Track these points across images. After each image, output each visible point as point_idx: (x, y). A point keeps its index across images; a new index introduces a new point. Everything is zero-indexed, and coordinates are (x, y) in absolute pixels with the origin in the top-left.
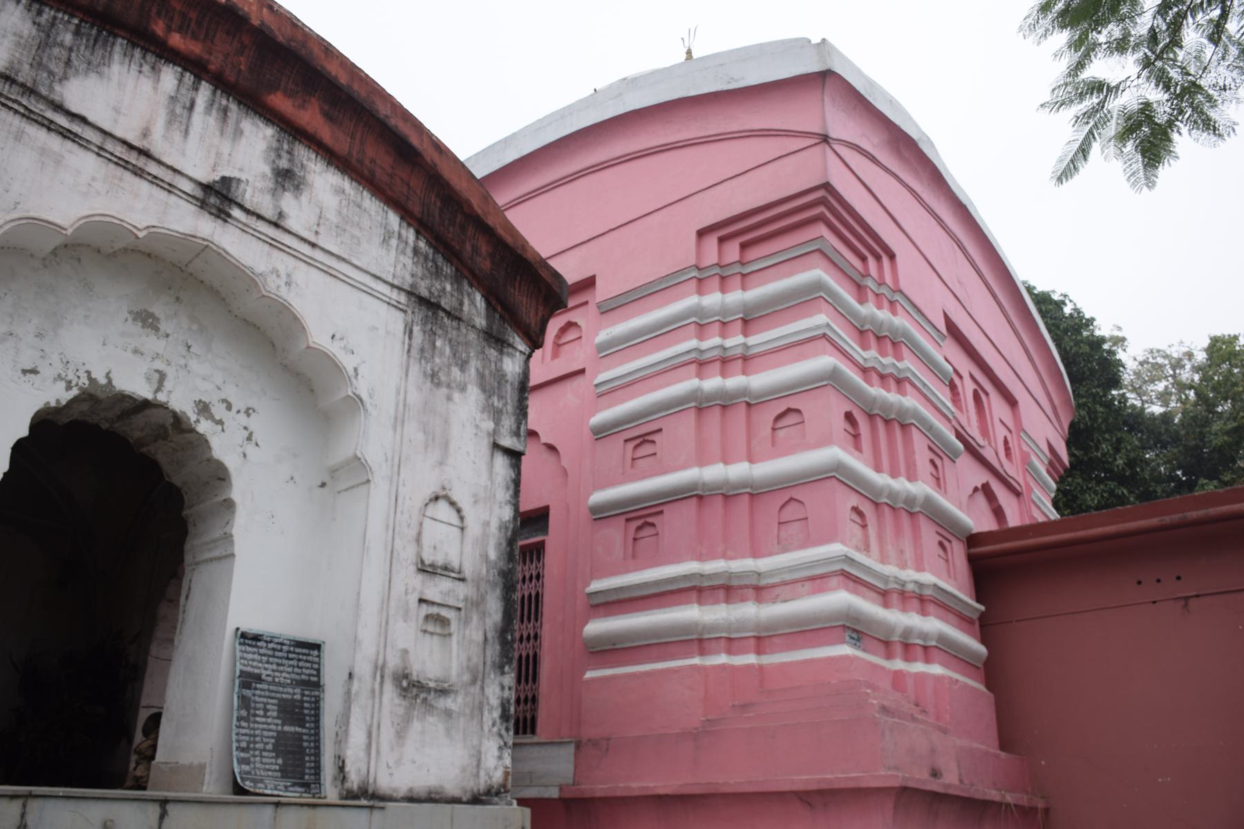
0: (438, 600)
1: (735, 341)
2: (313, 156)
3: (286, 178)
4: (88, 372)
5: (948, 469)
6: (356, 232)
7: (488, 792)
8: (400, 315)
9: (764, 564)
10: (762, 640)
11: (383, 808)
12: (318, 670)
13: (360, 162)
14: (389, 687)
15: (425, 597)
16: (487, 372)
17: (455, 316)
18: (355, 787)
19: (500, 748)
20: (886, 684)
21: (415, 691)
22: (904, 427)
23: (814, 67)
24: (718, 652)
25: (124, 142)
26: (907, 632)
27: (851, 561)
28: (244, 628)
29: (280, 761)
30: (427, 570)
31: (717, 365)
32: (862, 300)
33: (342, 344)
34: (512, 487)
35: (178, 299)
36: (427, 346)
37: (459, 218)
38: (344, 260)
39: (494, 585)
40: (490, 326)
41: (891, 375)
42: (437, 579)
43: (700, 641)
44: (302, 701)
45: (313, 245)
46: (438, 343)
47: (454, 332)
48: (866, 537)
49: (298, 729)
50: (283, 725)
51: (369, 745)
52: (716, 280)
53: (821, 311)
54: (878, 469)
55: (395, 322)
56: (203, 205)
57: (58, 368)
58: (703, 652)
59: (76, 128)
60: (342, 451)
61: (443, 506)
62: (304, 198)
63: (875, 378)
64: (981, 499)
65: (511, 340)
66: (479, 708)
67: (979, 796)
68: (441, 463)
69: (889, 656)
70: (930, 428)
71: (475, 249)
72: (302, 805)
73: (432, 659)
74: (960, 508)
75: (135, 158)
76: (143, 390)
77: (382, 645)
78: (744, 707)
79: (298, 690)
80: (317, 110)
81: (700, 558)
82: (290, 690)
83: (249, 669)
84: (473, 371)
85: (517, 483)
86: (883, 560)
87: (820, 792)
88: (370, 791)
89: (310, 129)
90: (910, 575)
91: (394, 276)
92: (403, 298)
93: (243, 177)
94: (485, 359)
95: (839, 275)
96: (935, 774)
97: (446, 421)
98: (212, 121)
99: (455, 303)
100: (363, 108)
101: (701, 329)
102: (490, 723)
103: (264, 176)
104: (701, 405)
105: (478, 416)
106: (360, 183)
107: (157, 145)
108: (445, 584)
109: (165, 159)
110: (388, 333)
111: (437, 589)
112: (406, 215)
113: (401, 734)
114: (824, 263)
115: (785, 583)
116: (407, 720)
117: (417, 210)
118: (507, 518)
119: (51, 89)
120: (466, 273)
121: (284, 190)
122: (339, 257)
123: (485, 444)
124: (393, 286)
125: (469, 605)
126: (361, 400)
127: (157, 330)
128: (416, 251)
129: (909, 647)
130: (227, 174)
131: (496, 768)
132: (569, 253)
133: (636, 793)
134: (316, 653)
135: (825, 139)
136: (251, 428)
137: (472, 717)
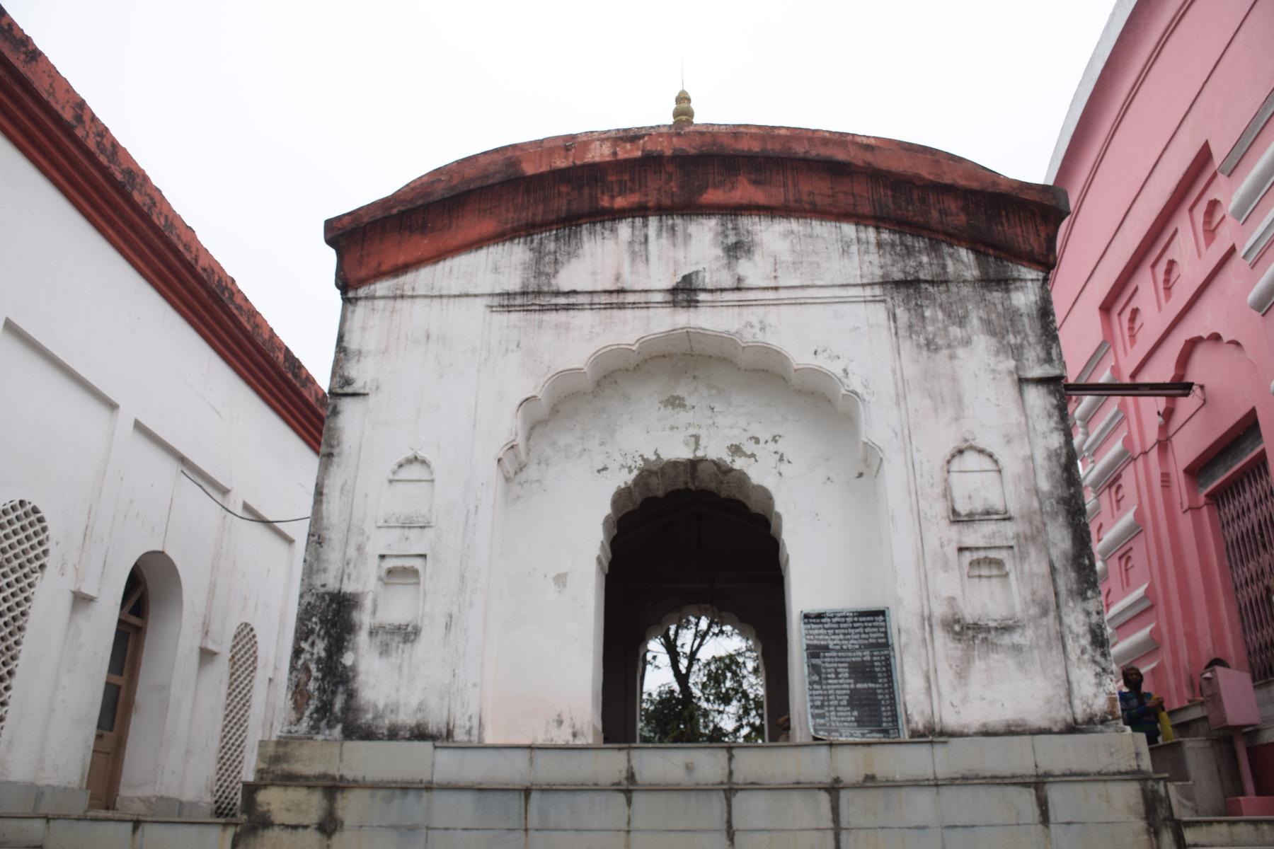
0: (981, 544)
2: (757, 219)
3: (736, 249)
4: (641, 456)
6: (814, 258)
11: (945, 742)
12: (886, 633)
13: (798, 201)
14: (939, 634)
15: (964, 545)
16: (993, 316)
17: (941, 281)
18: (920, 727)
19: (1097, 675)
21: (970, 633)
28: (806, 611)
29: (856, 713)
33: (826, 355)
34: (1056, 413)
35: (694, 377)
36: (914, 321)
37: (916, 194)
38: (808, 286)
40: (985, 272)
42: (976, 526)
44: (872, 661)
45: (776, 288)
46: (928, 313)
47: (944, 296)
49: (871, 685)
50: (855, 683)
51: (929, 688)
55: (878, 313)
56: (675, 304)
57: (620, 460)
59: (572, 300)
62: (757, 256)
65: (1016, 274)
71: (944, 212)
72: (856, 744)
73: (986, 600)
75: (616, 298)
76: (683, 453)
77: (925, 597)
79: (867, 653)
80: (746, 182)
82: (859, 654)
83: (815, 642)
84: (975, 322)
88: (938, 729)
89: (745, 202)
91: (861, 277)
92: (878, 291)
93: (700, 268)
97: (954, 379)
98: (665, 241)
99: (936, 269)
100: (782, 159)
102: (1079, 652)
103: (717, 258)
105: (992, 360)
106: (806, 218)
107: (629, 281)
108: (988, 528)
110: (871, 326)
111: (976, 536)
112: (858, 219)
116: (967, 661)
117: (867, 209)
118: (1057, 445)
119: (550, 284)
120: (941, 237)
121: (737, 258)
122: (802, 287)
124: (863, 285)
125: (1022, 541)
126: (856, 394)
127: (684, 406)
130: (686, 272)
131: (1095, 696)
132: (1180, 132)
134: (881, 618)
136: (780, 451)
137: (1049, 647)
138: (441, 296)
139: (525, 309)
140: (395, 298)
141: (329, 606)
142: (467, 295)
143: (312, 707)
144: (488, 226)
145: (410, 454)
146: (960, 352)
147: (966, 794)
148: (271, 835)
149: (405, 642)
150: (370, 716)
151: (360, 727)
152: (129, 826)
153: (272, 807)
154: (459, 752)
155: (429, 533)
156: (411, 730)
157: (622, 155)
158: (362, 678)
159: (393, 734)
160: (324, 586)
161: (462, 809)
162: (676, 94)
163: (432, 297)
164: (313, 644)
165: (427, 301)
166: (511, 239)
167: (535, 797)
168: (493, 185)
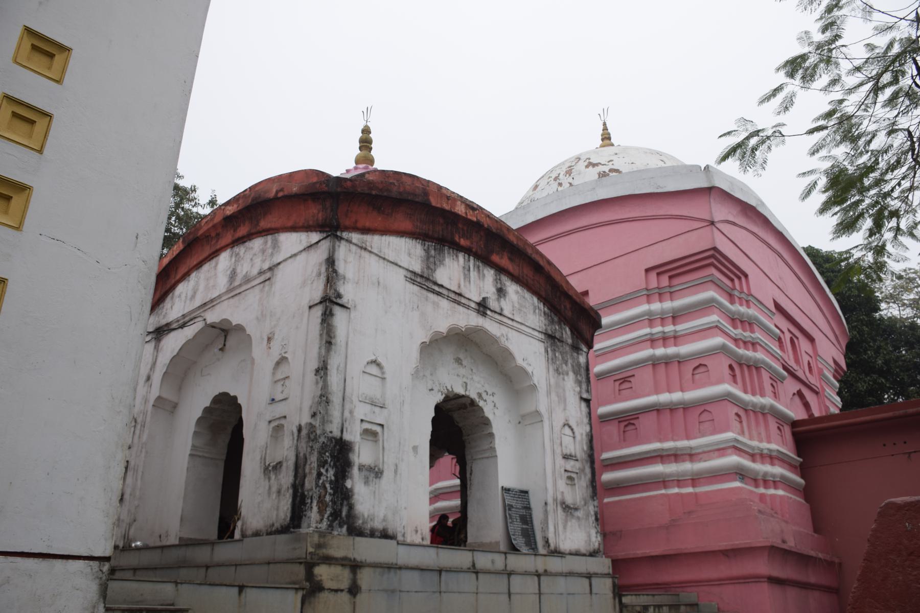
1: (669, 328)
5: (780, 388)
6: (525, 310)
7: (594, 552)
9: (693, 443)
10: (695, 480)
14: (559, 508)
17: (561, 341)
20: (757, 500)
22: (758, 369)
23: (704, 184)
24: (673, 487)
25: (454, 292)
26: (766, 474)
30: (566, 457)
31: (661, 341)
32: (732, 302)
39: (587, 461)
41: (749, 342)
43: (664, 482)
45: (513, 320)
48: (742, 427)
52: (657, 295)
53: (714, 313)
54: (746, 392)
56: (478, 311)
58: (665, 487)
59: (441, 290)
60: (529, 408)
61: (566, 427)
63: (741, 344)
64: (797, 399)
66: (588, 515)
67: (805, 553)
68: (565, 409)
69: (757, 486)
70: (771, 367)
71: (565, 306)
74: (787, 408)
75: (457, 298)
78: (690, 513)
81: (660, 441)
86: (751, 438)
87: (733, 550)
90: (765, 445)
95: (720, 290)
96: (784, 542)
97: (564, 390)
98: (476, 273)
101: (651, 322)
104: (655, 362)
108: (572, 463)
109: (467, 296)
111: (570, 465)
112: (540, 298)
113: (565, 527)
114: (713, 286)
115: (704, 452)
116: (566, 522)
123: (578, 398)
128: (545, 313)
129: (767, 481)
133: (640, 556)
135: (712, 223)
138: (384, 259)
139: (421, 286)
140: (361, 248)
141: (335, 446)
142: (396, 264)
143: (328, 512)
144: (407, 225)
145: (373, 358)
146: (566, 378)
147: (570, 580)
148: (324, 596)
150: (360, 522)
151: (355, 528)
152: (236, 590)
153: (323, 578)
155: (385, 411)
156: (381, 532)
157: (469, 217)
158: (356, 497)
159: (372, 534)
160: (331, 432)
164: (327, 471)
165: (377, 258)
166: (416, 239)
167: (443, 574)
168: (417, 202)
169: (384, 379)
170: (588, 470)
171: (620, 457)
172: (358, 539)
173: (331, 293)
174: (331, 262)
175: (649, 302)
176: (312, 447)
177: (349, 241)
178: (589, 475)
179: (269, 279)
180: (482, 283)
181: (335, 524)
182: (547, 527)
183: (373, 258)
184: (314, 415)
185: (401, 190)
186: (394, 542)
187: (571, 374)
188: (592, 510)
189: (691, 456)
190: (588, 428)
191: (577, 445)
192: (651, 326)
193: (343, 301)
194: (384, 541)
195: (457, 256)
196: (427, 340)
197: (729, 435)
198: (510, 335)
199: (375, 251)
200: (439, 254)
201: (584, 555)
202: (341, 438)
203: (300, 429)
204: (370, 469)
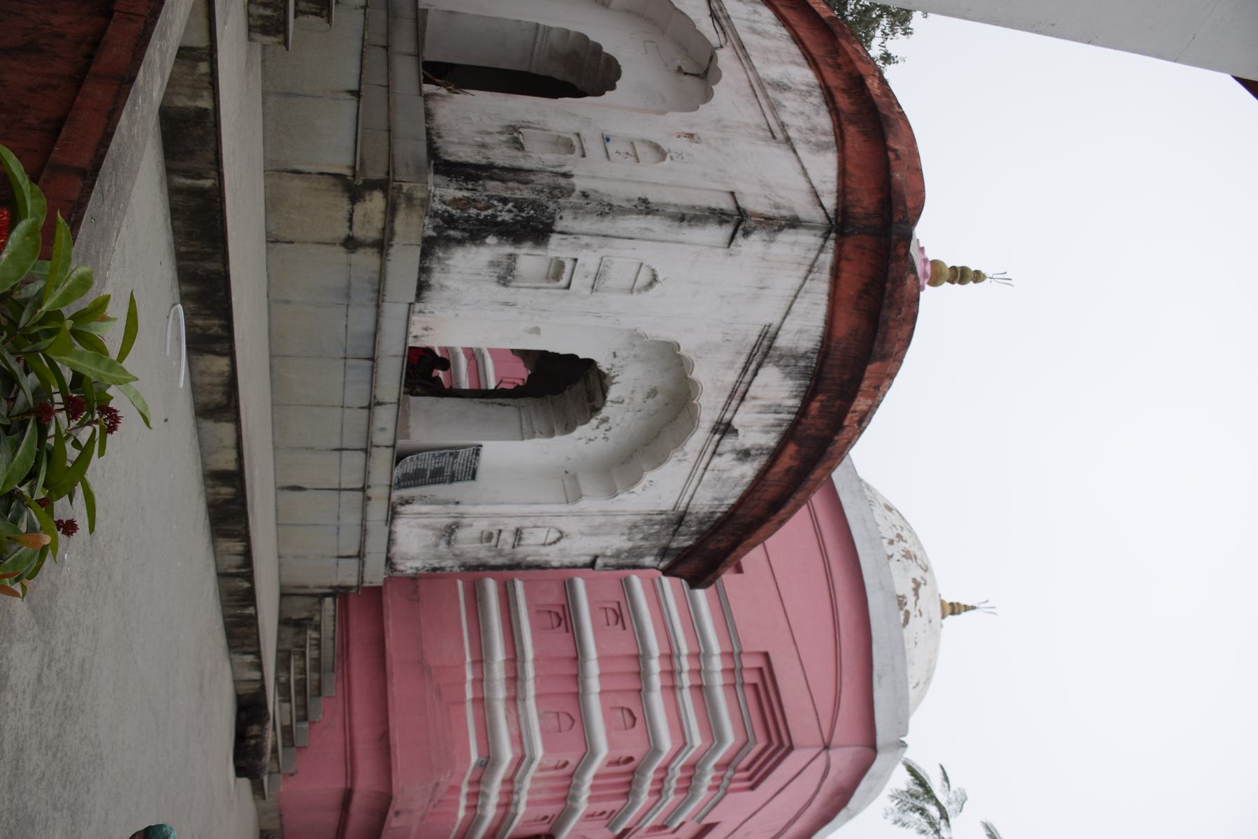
1: (686, 680)
8: (671, 507)
9: (531, 703)
10: (482, 703)
14: (450, 521)
17: (675, 533)
20: (453, 782)
23: (881, 739)
24: (474, 672)
25: (747, 391)
26: (486, 796)
27: (532, 761)
30: (518, 533)
31: (669, 668)
32: (718, 767)
39: (512, 560)
45: (706, 469)
53: (703, 741)
54: (596, 777)
56: (719, 423)
58: (474, 663)
59: (750, 373)
60: (586, 485)
63: (660, 775)
66: (440, 558)
68: (582, 534)
69: (471, 783)
70: (627, 812)
75: (739, 395)
78: (439, 693)
81: (536, 659)
84: (642, 543)
85: (575, 567)
86: (534, 780)
87: (388, 746)
90: (524, 798)
92: (682, 509)
94: (650, 548)
96: (397, 813)
97: (608, 534)
98: (771, 421)
101: (695, 656)
104: (641, 658)
108: (511, 540)
111: (508, 538)
112: (735, 508)
113: (426, 527)
115: (518, 717)
116: (434, 529)
123: (598, 552)
128: (713, 513)
129: (476, 796)
135: (827, 747)
138: (796, 297)
139: (757, 346)
140: (812, 266)
141: (542, 223)
142: (787, 313)
144: (841, 330)
145: (660, 278)
146: (625, 537)
147: (356, 531)
148: (344, 204)
149: (499, 277)
150: (441, 255)
151: (433, 248)
152: (355, 87)
154: (405, 317)
155: (587, 291)
157: (849, 415)
158: (474, 249)
159: (424, 270)
161: (362, 319)
162: (983, 271)
163: (799, 291)
164: (510, 211)
165: (797, 287)
166: (822, 342)
167: (369, 363)
169: (631, 291)
170: (499, 561)
171: (516, 604)
172: (418, 251)
173: (750, 223)
174: (794, 223)
175: (723, 654)
176: (542, 191)
177: (822, 249)
178: (493, 562)
179: (774, 137)
180: (757, 429)
181: (438, 220)
182: (427, 504)
183: (798, 282)
184: (585, 195)
185: (891, 324)
186: (412, 298)
187: (629, 545)
188: (448, 563)
189: (514, 699)
190: (556, 563)
191: (534, 547)
192: (690, 656)
193: (739, 239)
194: (415, 284)
195: (795, 397)
196: (682, 351)
197: (539, 752)
198: (684, 464)
199: (807, 285)
200: (800, 372)
201: (388, 550)
202: (553, 231)
203: (566, 175)
204: (510, 270)
